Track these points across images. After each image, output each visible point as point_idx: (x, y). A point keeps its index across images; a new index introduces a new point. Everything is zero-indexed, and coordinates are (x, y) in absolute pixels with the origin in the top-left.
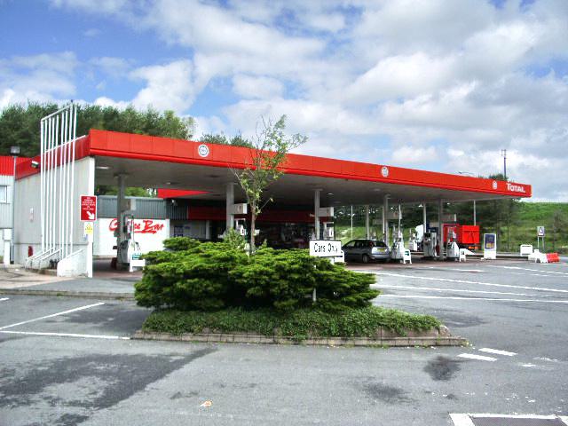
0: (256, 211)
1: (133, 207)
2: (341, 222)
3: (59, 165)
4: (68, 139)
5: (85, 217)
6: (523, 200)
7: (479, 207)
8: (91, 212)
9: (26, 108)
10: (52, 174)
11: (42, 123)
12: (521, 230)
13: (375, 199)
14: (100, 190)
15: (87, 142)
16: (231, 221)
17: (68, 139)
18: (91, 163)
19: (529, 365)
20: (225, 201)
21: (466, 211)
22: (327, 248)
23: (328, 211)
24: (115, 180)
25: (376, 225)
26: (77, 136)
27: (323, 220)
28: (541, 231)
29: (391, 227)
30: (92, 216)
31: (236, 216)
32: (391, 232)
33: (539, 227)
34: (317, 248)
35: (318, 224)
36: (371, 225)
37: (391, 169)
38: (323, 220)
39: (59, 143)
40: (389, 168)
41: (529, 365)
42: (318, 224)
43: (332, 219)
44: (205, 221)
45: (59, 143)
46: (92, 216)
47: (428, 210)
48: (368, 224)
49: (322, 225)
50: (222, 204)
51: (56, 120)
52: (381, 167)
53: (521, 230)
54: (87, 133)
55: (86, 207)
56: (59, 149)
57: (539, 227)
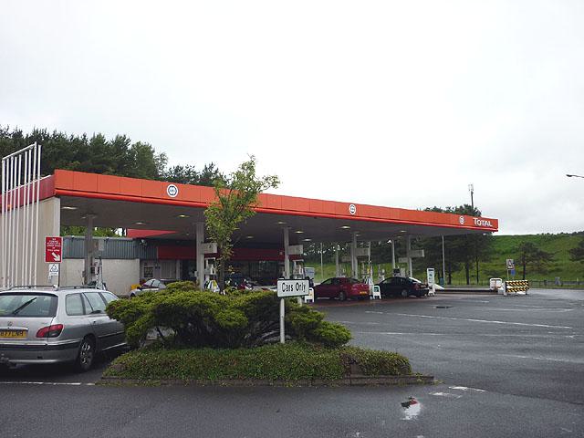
0: (227, 252)
1: (101, 248)
2: (311, 259)
3: (22, 206)
4: (32, 179)
5: (50, 258)
6: (494, 234)
7: (447, 241)
8: (56, 253)
9: (69, 137)
10: (16, 214)
11: (3, 162)
12: (490, 266)
13: (344, 238)
14: (65, 227)
15: (52, 182)
16: (200, 260)
17: (32, 179)
18: (57, 202)
19: (440, 394)
20: (195, 241)
21: (312, 258)
22: (294, 288)
23: (298, 249)
24: (83, 218)
25: (346, 262)
26: (41, 176)
27: (292, 258)
28: (510, 262)
29: (359, 264)
30: (57, 258)
31: (206, 256)
32: (360, 268)
33: (507, 260)
34: (285, 287)
35: (287, 262)
36: (340, 262)
37: (357, 206)
38: (292, 258)
39: (22, 183)
40: (357, 205)
41: (440, 394)
42: (287, 262)
43: (303, 257)
44: (176, 260)
45: (22, 183)
46: (57, 258)
47: (397, 245)
48: (337, 261)
49: (292, 265)
50: (192, 244)
51: (23, 158)
52: (350, 204)
53: (490, 266)
54: (52, 173)
55: (51, 248)
56: (22, 189)
57: (507, 260)
